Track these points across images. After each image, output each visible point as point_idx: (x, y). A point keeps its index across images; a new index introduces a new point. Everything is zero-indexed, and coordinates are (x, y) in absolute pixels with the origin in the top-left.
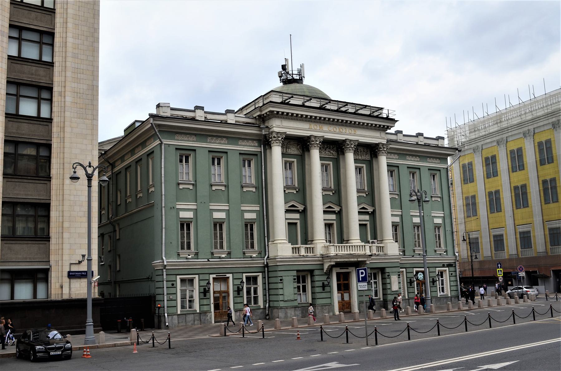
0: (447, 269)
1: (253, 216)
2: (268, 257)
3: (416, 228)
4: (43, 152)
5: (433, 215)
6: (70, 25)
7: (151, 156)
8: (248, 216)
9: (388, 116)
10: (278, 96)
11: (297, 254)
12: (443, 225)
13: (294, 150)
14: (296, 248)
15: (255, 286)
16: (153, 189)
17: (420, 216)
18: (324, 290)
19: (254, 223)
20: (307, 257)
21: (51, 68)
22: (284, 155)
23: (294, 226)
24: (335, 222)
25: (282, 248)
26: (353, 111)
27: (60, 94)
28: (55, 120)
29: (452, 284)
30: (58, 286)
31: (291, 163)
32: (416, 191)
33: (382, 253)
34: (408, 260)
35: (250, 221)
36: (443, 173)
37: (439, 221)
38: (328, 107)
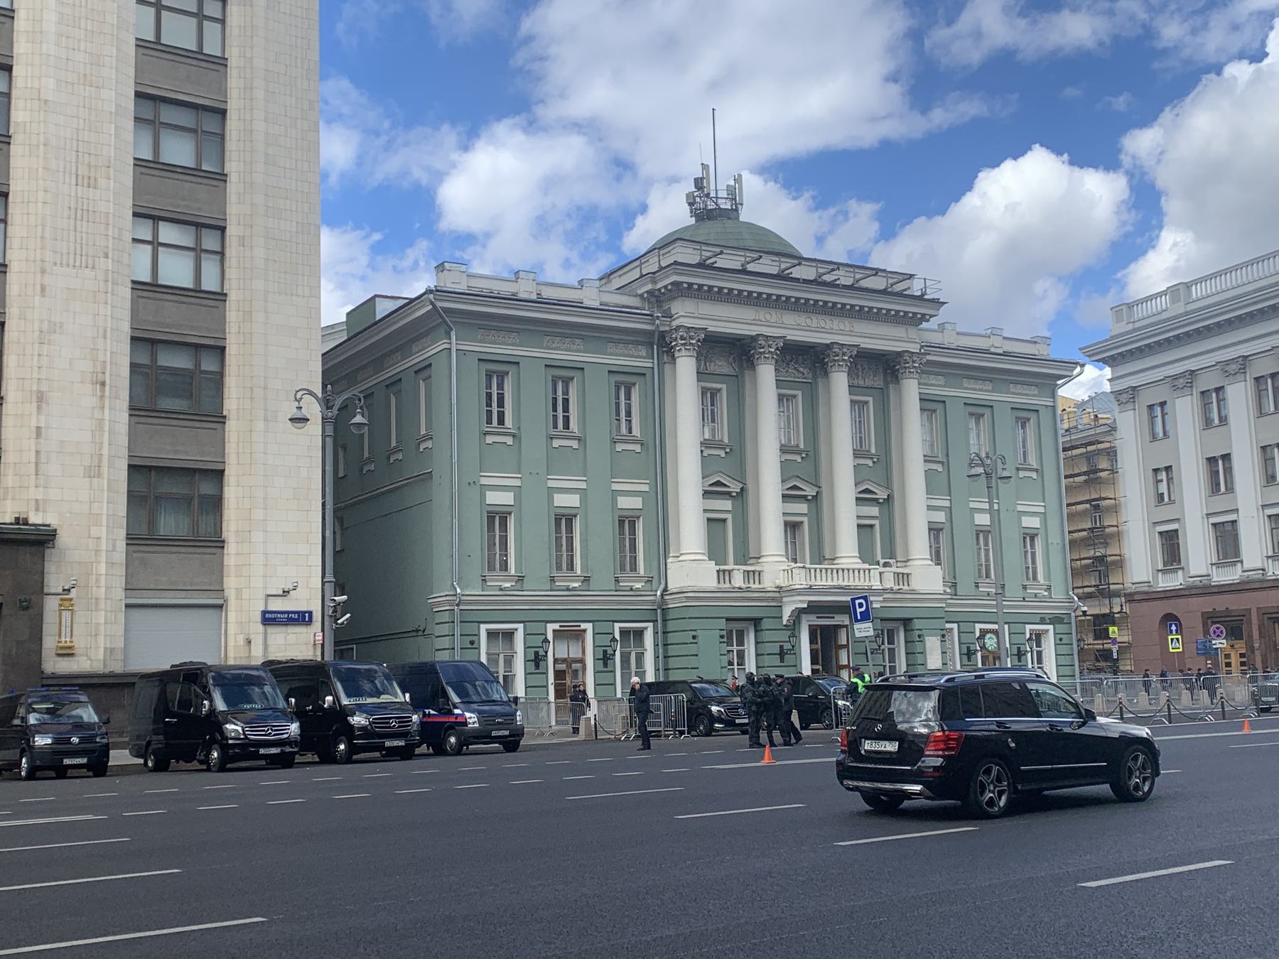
0: (1051, 627)
1: (636, 503)
2: (665, 590)
3: (563, 521)
4: (208, 365)
5: (1020, 508)
6: (259, 94)
7: (424, 374)
8: (625, 503)
9: (923, 295)
10: (691, 251)
11: (727, 585)
12: (1042, 532)
13: (721, 366)
14: (724, 571)
15: (639, 650)
16: (429, 444)
17: (990, 511)
18: (782, 660)
19: (510, 513)
20: (748, 590)
21: (221, 184)
22: (701, 375)
23: (718, 526)
24: (805, 519)
25: (691, 569)
26: (849, 282)
27: (242, 241)
28: (233, 297)
29: (1063, 660)
30: (241, 640)
31: (714, 393)
32: (983, 455)
33: (906, 588)
34: (958, 606)
35: (630, 513)
36: (1045, 416)
37: (1032, 522)
38: (797, 272)
